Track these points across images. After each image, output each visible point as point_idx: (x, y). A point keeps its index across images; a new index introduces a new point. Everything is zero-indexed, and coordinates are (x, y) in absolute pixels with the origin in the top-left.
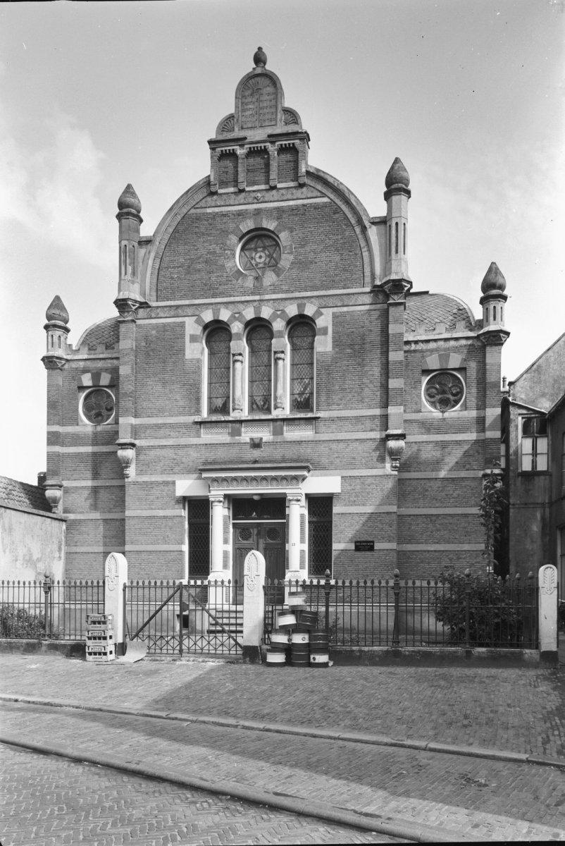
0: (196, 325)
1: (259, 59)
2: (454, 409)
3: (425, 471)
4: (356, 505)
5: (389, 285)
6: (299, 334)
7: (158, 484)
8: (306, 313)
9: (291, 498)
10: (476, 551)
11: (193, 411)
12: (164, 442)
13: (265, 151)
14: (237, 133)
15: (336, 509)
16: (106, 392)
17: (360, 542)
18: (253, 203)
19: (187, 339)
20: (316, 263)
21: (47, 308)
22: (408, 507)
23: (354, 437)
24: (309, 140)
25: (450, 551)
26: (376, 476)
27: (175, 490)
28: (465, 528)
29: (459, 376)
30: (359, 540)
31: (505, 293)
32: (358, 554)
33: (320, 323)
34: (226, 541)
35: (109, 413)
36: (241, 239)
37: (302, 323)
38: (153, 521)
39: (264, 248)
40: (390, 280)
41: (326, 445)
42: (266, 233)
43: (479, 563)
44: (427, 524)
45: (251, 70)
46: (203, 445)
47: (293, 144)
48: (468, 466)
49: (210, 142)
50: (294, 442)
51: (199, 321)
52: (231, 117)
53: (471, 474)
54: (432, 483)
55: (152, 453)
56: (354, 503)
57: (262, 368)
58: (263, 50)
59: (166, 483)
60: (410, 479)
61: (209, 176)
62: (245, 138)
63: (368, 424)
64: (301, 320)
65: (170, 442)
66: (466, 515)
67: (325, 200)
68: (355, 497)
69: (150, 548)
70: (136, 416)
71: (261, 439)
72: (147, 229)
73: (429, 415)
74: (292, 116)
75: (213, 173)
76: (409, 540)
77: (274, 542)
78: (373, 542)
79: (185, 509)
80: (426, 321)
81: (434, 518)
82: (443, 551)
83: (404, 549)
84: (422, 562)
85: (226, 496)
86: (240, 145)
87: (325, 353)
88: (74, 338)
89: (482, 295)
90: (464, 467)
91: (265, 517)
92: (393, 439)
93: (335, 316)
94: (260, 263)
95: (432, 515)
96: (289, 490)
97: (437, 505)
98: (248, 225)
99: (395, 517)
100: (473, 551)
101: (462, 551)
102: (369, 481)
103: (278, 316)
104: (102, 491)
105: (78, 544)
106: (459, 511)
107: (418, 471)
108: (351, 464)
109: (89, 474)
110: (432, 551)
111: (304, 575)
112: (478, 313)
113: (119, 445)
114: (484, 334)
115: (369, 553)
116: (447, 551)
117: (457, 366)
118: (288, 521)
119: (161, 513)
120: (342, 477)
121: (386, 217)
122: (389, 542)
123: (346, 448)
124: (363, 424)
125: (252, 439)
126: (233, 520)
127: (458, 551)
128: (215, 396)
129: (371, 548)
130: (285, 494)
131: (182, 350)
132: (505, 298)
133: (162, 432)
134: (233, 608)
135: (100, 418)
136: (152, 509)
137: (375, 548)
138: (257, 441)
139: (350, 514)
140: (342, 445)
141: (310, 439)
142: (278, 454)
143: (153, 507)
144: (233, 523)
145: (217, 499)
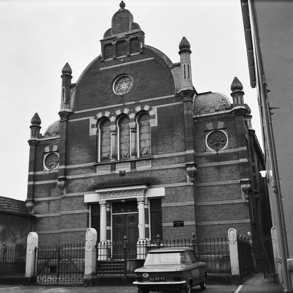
0: (94, 120)
1: (122, 5)
2: (223, 149)
3: (210, 182)
4: (173, 202)
5: (182, 93)
6: (143, 119)
7: (76, 196)
8: (105, 116)
9: (101, 203)
10: (241, 223)
12: (79, 176)
14: (113, 36)
15: (163, 205)
16: (56, 154)
17: (176, 222)
19: (90, 126)
20: (149, 86)
21: (194, 86)
22: (203, 202)
23: (170, 167)
24: (144, 34)
25: (227, 224)
26: (182, 186)
27: (84, 200)
28: (234, 211)
29: (224, 132)
30: (176, 220)
32: (176, 228)
33: (151, 113)
34: (146, 222)
35: (57, 164)
37: (145, 113)
38: (73, 216)
39: (126, 81)
40: (182, 91)
41: (157, 172)
42: (126, 75)
43: (243, 230)
44: (213, 210)
45: (118, 10)
46: (97, 176)
47: (124, 40)
48: (232, 178)
49: (101, 41)
50: (141, 171)
52: (110, 30)
53: (234, 182)
54: (214, 188)
55: (77, 181)
56: (172, 201)
57: (126, 137)
58: (124, 2)
59: (80, 196)
60: (206, 186)
61: (100, 55)
62: (116, 37)
63: (177, 160)
64: (143, 113)
65: (82, 176)
66: (234, 204)
68: (172, 198)
69: (72, 230)
71: (125, 171)
72: (74, 80)
73: (209, 153)
74: (136, 26)
75: (102, 54)
76: (205, 219)
77: (133, 224)
78: (183, 221)
79: (89, 209)
80: (207, 107)
81: (216, 207)
82: (223, 224)
83: (202, 224)
84: (212, 231)
85: (107, 201)
86: (113, 41)
87: (155, 127)
89: (232, 92)
90: (230, 178)
91: (129, 211)
92: (189, 167)
95: (215, 205)
96: (139, 197)
97: (218, 199)
99: (193, 207)
100: (239, 223)
101: (233, 224)
102: (179, 189)
104: (52, 202)
105: (40, 229)
106: (230, 202)
107: (206, 182)
108: (169, 182)
109: (46, 194)
110: (217, 225)
112: (231, 100)
113: (58, 179)
114: (233, 111)
115: (181, 228)
116: (225, 224)
117: (222, 127)
118: (138, 212)
119: (77, 212)
120: (165, 188)
121: (180, 63)
122: (191, 221)
123: (167, 172)
124: (174, 160)
125: (120, 172)
126: (113, 213)
127: (231, 224)
128: (104, 152)
129: (182, 225)
130: (136, 198)
131: (88, 131)
133: (78, 171)
136: (73, 210)
137: (184, 224)
138: (123, 173)
139: (170, 207)
140: (164, 172)
141: (149, 169)
142: (133, 177)
143: (73, 209)
144: (113, 215)
145: (103, 203)
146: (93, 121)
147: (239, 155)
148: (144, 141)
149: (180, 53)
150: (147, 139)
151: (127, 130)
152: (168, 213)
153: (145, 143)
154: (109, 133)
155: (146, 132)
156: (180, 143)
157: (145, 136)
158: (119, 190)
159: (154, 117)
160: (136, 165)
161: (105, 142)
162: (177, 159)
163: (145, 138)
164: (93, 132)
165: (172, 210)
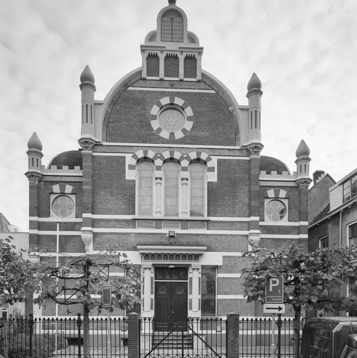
11: (131, 212)
13: (176, 57)
18: (210, 90)
31: (310, 156)
36: (161, 109)
49: (142, 46)
51: (134, 156)
55: (104, 237)
62: (164, 47)
67: (213, 92)
70: (93, 213)
74: (192, 38)
88: (46, 161)
93: (219, 162)
94: (171, 125)
98: (165, 101)
103: (159, 157)
111: (198, 314)
132: (309, 160)
133: (110, 224)
134: (273, 346)
135: (64, 213)
146: (129, 160)
147: (299, 230)
148: (195, 198)
149: (81, 86)
150: (200, 196)
151: (174, 181)
152: (225, 285)
153: (197, 200)
154: (149, 181)
155: (198, 187)
156: (243, 207)
157: (197, 192)
158: (164, 253)
159: (212, 169)
160: (162, 226)
161: (145, 192)
162: (238, 225)
163: (197, 195)
164: (130, 175)
165: (229, 281)
